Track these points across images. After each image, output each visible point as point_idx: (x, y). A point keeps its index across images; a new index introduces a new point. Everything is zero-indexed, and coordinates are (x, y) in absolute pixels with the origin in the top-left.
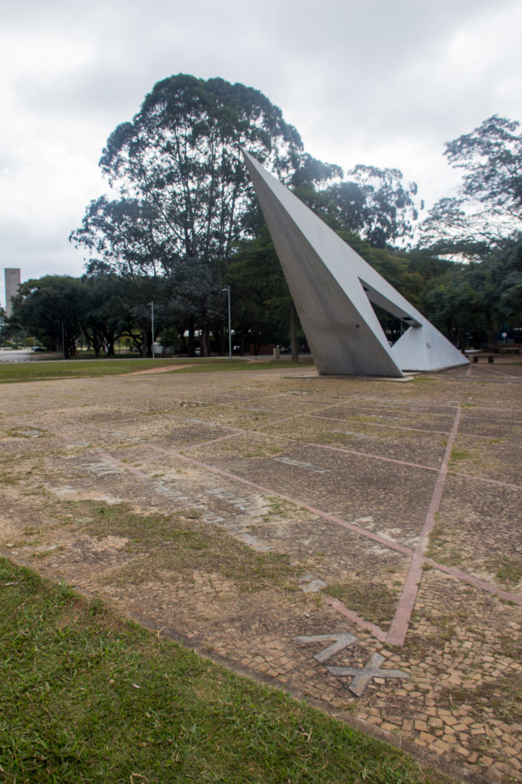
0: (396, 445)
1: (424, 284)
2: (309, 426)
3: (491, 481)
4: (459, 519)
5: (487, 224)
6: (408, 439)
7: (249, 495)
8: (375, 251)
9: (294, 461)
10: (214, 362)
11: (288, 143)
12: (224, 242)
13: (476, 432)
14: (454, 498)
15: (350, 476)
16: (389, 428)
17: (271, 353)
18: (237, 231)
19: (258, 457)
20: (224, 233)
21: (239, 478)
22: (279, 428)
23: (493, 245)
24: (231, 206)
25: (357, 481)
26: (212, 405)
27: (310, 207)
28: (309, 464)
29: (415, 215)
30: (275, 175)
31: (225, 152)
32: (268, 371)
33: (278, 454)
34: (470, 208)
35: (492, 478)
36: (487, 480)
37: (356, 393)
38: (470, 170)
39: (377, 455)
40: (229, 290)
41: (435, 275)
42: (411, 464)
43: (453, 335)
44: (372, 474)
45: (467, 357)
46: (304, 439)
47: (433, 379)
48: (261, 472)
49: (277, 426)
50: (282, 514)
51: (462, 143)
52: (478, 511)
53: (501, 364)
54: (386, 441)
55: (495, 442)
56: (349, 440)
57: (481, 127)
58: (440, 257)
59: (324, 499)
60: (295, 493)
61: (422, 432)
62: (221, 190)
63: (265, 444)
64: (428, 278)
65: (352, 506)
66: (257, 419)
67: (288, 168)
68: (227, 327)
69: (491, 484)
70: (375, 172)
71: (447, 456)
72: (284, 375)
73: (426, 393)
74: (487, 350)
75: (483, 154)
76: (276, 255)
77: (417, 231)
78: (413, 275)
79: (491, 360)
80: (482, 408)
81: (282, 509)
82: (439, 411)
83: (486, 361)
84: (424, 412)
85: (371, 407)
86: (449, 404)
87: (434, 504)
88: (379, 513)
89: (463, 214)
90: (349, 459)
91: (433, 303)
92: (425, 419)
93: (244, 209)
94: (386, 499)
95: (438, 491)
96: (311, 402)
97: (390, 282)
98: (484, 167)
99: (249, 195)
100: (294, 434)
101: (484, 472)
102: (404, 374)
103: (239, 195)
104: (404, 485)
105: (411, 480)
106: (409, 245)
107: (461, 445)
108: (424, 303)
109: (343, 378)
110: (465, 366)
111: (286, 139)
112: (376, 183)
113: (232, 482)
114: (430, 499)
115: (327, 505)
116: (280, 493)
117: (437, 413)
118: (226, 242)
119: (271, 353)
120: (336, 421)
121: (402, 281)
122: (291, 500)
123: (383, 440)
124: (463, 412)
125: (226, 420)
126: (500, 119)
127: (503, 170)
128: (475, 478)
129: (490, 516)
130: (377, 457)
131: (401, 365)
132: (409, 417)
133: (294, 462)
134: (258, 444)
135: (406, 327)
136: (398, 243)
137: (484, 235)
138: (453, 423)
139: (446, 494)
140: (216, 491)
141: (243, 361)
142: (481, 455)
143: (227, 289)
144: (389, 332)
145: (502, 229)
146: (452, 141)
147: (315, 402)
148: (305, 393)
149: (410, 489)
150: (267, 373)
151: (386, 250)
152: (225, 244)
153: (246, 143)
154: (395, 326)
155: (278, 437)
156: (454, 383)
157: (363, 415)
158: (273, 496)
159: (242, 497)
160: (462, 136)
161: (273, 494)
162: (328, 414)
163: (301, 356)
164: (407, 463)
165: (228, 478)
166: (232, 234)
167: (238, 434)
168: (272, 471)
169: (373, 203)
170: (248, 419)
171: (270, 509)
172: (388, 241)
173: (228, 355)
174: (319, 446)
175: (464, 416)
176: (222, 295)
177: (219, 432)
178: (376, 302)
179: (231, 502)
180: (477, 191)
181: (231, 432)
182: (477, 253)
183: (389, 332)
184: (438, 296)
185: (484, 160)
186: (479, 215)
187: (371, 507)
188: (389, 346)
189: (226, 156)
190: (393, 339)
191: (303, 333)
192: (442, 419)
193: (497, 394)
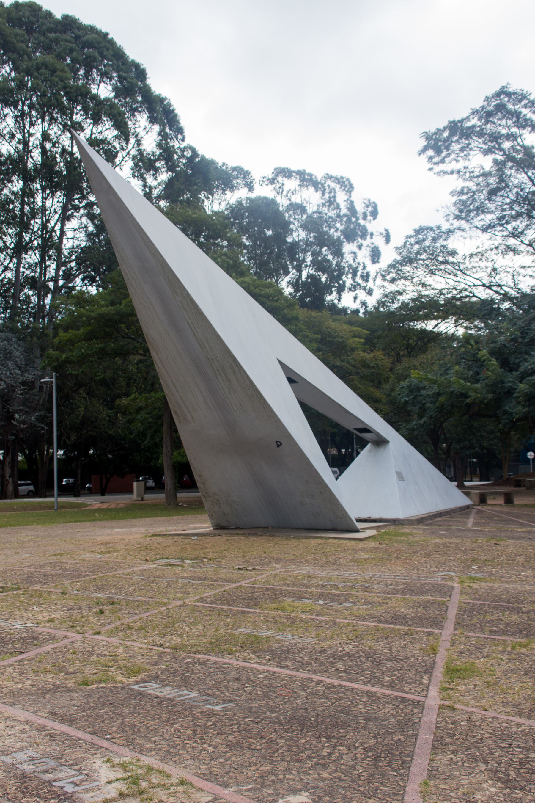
0: (348, 654)
1: (391, 370)
2: (195, 623)
3: (517, 719)
4: (464, 794)
5: (494, 270)
6: (369, 643)
7: (84, 759)
8: (307, 315)
9: (168, 688)
10: (25, 508)
11: (157, 128)
12: (46, 295)
13: (487, 628)
14: (454, 752)
15: (268, 714)
16: (335, 623)
17: (131, 491)
18: (69, 276)
19: (103, 685)
20: (45, 281)
21: (64, 728)
22: (141, 628)
23: (506, 305)
24: (58, 233)
25: (281, 724)
26: (18, 589)
27: (195, 239)
28: (194, 694)
29: (375, 255)
30: (137, 184)
31: (46, 137)
32: (123, 522)
33: (139, 678)
34: (466, 243)
35: (520, 714)
36: (511, 718)
37: (278, 561)
38: (465, 180)
39: (315, 673)
40: (54, 380)
41: (409, 355)
42: (374, 689)
43: (443, 456)
44: (306, 709)
45: (467, 494)
46: (185, 646)
47: (410, 534)
48: (106, 713)
49: (138, 624)
50: (145, 796)
51: (451, 135)
52: (499, 780)
53: (526, 506)
54: (330, 647)
55: (521, 646)
56: (266, 646)
57: (483, 107)
58: (420, 325)
59: (221, 760)
60: (168, 751)
61: (393, 630)
62: (40, 204)
63: (115, 658)
64: (398, 359)
65: (272, 772)
66: (102, 612)
67: (156, 170)
68: (50, 444)
69: (519, 725)
70: (306, 179)
71: (439, 672)
72: (152, 532)
73: (397, 558)
74: (500, 481)
75: (486, 152)
76: (138, 321)
77: (379, 281)
78: (371, 355)
79: (509, 500)
80: (496, 585)
81: (144, 784)
82: (421, 591)
83: (501, 501)
84: (395, 592)
85: (303, 585)
86: (437, 578)
87: (419, 766)
88: (321, 784)
89: (453, 253)
90: (266, 682)
91: (406, 402)
92: (399, 605)
93: (82, 240)
94: (333, 757)
95: (426, 738)
96: (199, 578)
97: (333, 368)
98: (486, 175)
99: (91, 217)
100: (168, 638)
101: (505, 704)
102: (359, 525)
103: (72, 216)
104: (365, 728)
105: (376, 719)
106: (364, 304)
107: (461, 653)
108: (392, 402)
109: (255, 534)
110: (465, 510)
111: (153, 120)
112: (312, 199)
113: (51, 736)
114: (411, 755)
115: (227, 773)
116: (141, 752)
117: (417, 594)
118: (50, 296)
119: (131, 491)
120: (243, 612)
121: (354, 366)
122: (161, 766)
123: (326, 644)
124: (462, 593)
125: (46, 616)
126: (514, 94)
127: (519, 178)
128: (490, 714)
129: (522, 788)
130: (316, 678)
131: (354, 511)
132: (369, 603)
133: (167, 692)
134: (102, 659)
135: (363, 444)
136: (347, 301)
137: (489, 287)
138: (446, 612)
139: (439, 744)
140: (21, 756)
141: (78, 506)
142: (498, 671)
143: (50, 379)
144: (334, 452)
145: (521, 278)
146: (433, 130)
147: (206, 579)
148: (188, 562)
149: (375, 737)
150: (121, 527)
151: (326, 313)
152: (48, 300)
153: (85, 126)
154: (342, 443)
155: (138, 645)
156: (447, 540)
157: (289, 601)
158: (127, 759)
159: (70, 766)
160: (450, 122)
161: (127, 755)
162: (228, 599)
163: (182, 495)
164: (368, 688)
165: (44, 728)
166: (61, 283)
167: (66, 642)
168: (126, 711)
169: (303, 235)
170: (85, 612)
171: (121, 786)
172: (328, 298)
173: (52, 496)
174: (213, 659)
175: (466, 599)
176: (41, 388)
177: (32, 639)
178: (310, 403)
179: (48, 777)
180: (477, 215)
181: (52, 638)
182: (478, 317)
183: (334, 452)
184: (415, 390)
185: (487, 163)
186: (481, 255)
187: (306, 773)
188: (333, 477)
189: (48, 145)
190: (340, 463)
191: (184, 455)
192: (426, 605)
193: (521, 559)
